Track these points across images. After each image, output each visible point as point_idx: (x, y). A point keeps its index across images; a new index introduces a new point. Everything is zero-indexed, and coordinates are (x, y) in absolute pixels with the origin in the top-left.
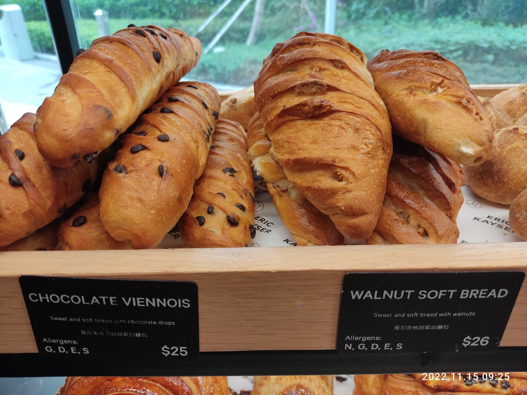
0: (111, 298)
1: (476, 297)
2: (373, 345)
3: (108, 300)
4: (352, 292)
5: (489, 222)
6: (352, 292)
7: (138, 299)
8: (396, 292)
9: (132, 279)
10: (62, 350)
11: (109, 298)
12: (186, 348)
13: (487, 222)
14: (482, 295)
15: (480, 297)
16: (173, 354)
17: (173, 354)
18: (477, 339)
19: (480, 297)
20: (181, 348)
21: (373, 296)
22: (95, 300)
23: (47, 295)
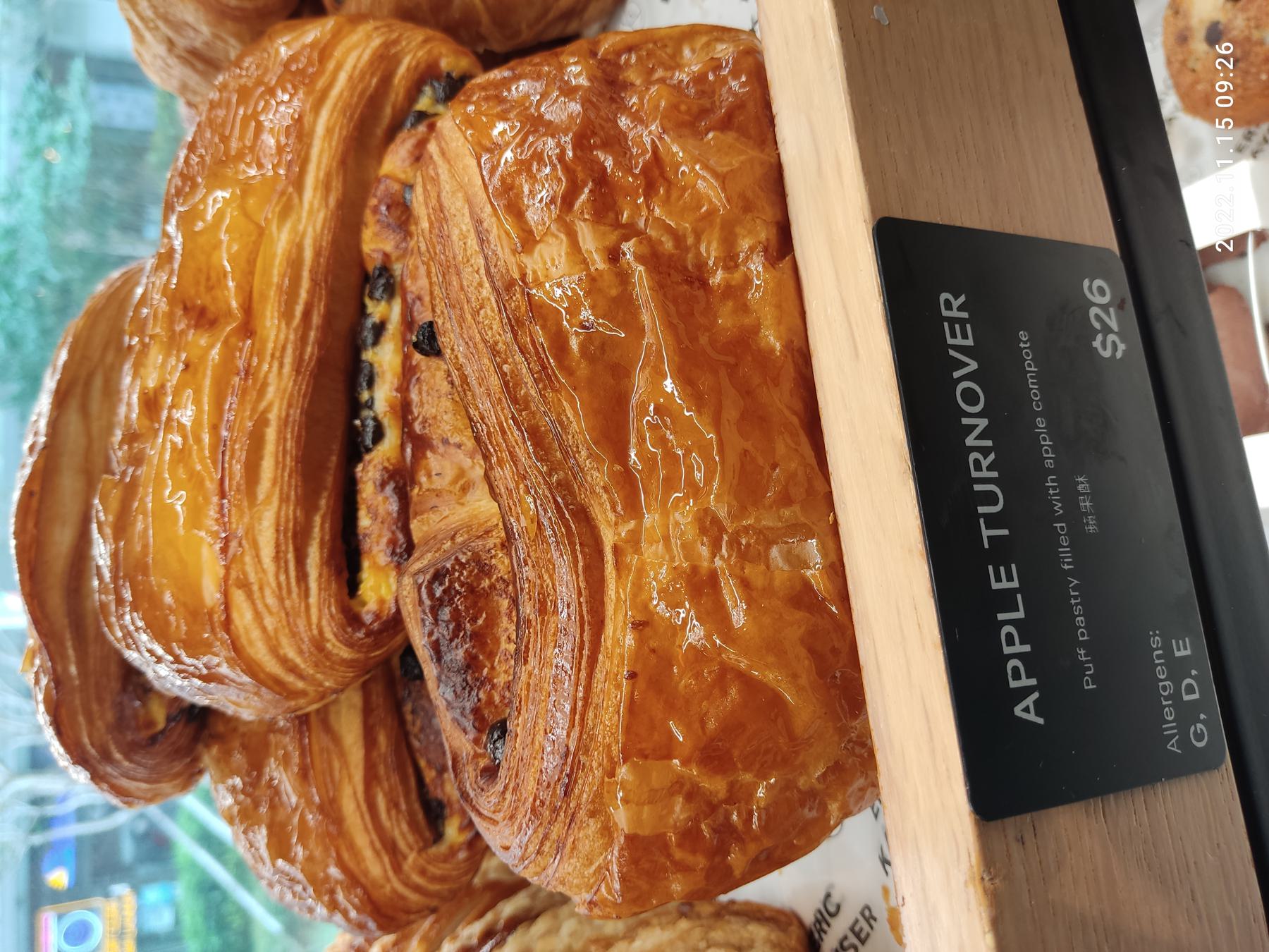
1: (992, 457)
2: (1186, 698)
11: (984, 515)
12: (990, 568)
14: (965, 336)
16: (1114, 324)
18: (1098, 317)
22: (1027, 710)
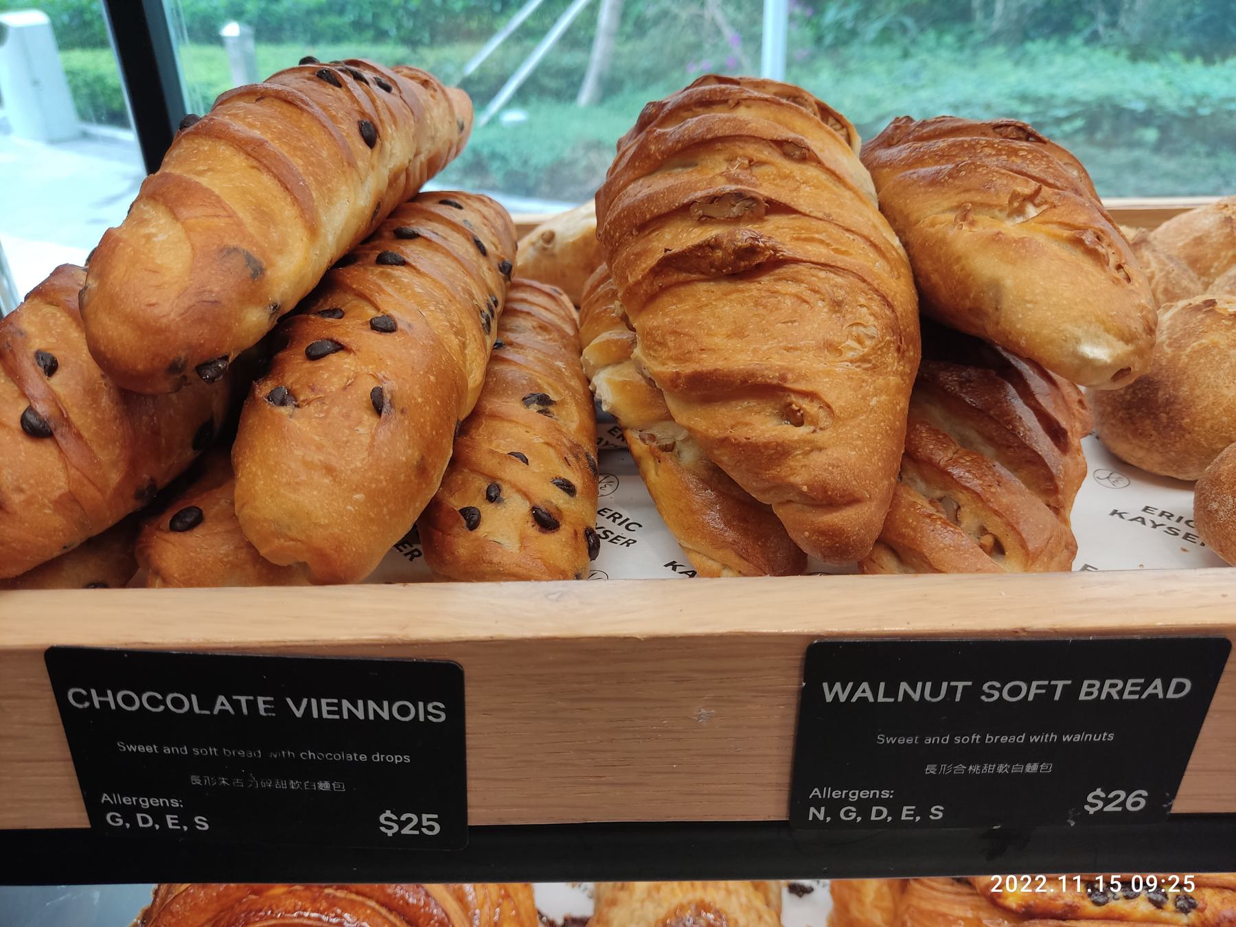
0: (260, 700)
1: (1116, 697)
2: (874, 809)
3: (252, 705)
4: (825, 685)
5: (1147, 521)
6: (825, 685)
7: (324, 701)
8: (929, 685)
9: (310, 654)
10: (145, 821)
11: (256, 700)
12: (436, 816)
13: (1143, 522)
14: (1131, 693)
15: (1126, 696)
16: (406, 831)
17: (406, 831)
18: (1118, 797)
19: (1126, 696)
20: (425, 817)
21: (875, 695)
22: (223, 704)
23: (109, 693)
